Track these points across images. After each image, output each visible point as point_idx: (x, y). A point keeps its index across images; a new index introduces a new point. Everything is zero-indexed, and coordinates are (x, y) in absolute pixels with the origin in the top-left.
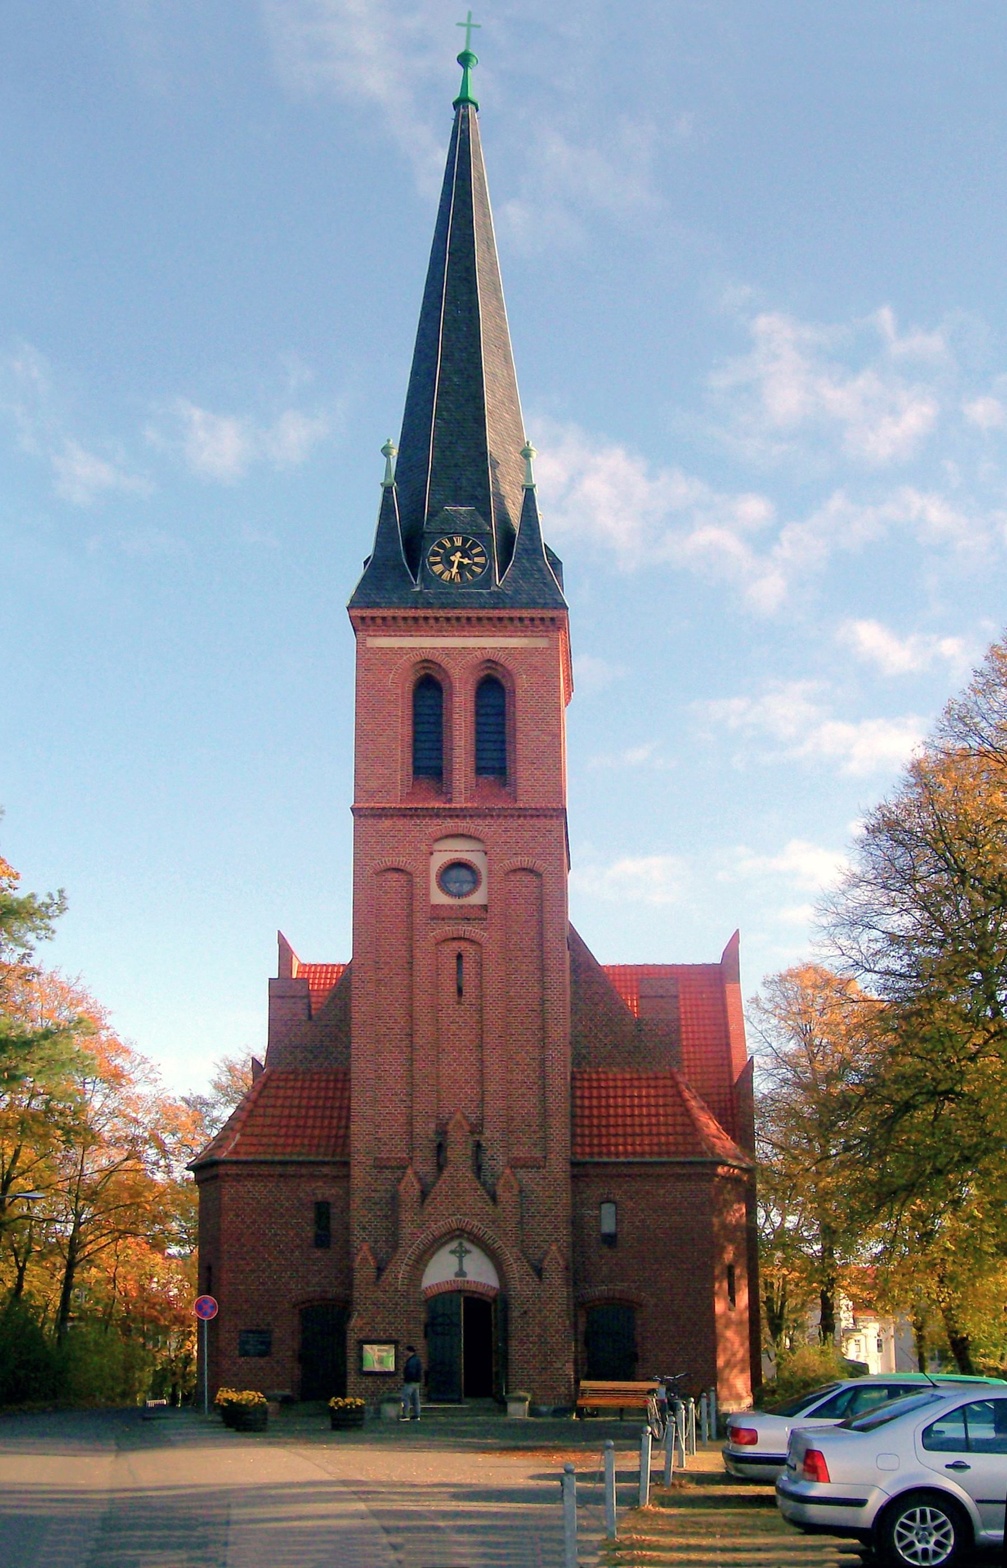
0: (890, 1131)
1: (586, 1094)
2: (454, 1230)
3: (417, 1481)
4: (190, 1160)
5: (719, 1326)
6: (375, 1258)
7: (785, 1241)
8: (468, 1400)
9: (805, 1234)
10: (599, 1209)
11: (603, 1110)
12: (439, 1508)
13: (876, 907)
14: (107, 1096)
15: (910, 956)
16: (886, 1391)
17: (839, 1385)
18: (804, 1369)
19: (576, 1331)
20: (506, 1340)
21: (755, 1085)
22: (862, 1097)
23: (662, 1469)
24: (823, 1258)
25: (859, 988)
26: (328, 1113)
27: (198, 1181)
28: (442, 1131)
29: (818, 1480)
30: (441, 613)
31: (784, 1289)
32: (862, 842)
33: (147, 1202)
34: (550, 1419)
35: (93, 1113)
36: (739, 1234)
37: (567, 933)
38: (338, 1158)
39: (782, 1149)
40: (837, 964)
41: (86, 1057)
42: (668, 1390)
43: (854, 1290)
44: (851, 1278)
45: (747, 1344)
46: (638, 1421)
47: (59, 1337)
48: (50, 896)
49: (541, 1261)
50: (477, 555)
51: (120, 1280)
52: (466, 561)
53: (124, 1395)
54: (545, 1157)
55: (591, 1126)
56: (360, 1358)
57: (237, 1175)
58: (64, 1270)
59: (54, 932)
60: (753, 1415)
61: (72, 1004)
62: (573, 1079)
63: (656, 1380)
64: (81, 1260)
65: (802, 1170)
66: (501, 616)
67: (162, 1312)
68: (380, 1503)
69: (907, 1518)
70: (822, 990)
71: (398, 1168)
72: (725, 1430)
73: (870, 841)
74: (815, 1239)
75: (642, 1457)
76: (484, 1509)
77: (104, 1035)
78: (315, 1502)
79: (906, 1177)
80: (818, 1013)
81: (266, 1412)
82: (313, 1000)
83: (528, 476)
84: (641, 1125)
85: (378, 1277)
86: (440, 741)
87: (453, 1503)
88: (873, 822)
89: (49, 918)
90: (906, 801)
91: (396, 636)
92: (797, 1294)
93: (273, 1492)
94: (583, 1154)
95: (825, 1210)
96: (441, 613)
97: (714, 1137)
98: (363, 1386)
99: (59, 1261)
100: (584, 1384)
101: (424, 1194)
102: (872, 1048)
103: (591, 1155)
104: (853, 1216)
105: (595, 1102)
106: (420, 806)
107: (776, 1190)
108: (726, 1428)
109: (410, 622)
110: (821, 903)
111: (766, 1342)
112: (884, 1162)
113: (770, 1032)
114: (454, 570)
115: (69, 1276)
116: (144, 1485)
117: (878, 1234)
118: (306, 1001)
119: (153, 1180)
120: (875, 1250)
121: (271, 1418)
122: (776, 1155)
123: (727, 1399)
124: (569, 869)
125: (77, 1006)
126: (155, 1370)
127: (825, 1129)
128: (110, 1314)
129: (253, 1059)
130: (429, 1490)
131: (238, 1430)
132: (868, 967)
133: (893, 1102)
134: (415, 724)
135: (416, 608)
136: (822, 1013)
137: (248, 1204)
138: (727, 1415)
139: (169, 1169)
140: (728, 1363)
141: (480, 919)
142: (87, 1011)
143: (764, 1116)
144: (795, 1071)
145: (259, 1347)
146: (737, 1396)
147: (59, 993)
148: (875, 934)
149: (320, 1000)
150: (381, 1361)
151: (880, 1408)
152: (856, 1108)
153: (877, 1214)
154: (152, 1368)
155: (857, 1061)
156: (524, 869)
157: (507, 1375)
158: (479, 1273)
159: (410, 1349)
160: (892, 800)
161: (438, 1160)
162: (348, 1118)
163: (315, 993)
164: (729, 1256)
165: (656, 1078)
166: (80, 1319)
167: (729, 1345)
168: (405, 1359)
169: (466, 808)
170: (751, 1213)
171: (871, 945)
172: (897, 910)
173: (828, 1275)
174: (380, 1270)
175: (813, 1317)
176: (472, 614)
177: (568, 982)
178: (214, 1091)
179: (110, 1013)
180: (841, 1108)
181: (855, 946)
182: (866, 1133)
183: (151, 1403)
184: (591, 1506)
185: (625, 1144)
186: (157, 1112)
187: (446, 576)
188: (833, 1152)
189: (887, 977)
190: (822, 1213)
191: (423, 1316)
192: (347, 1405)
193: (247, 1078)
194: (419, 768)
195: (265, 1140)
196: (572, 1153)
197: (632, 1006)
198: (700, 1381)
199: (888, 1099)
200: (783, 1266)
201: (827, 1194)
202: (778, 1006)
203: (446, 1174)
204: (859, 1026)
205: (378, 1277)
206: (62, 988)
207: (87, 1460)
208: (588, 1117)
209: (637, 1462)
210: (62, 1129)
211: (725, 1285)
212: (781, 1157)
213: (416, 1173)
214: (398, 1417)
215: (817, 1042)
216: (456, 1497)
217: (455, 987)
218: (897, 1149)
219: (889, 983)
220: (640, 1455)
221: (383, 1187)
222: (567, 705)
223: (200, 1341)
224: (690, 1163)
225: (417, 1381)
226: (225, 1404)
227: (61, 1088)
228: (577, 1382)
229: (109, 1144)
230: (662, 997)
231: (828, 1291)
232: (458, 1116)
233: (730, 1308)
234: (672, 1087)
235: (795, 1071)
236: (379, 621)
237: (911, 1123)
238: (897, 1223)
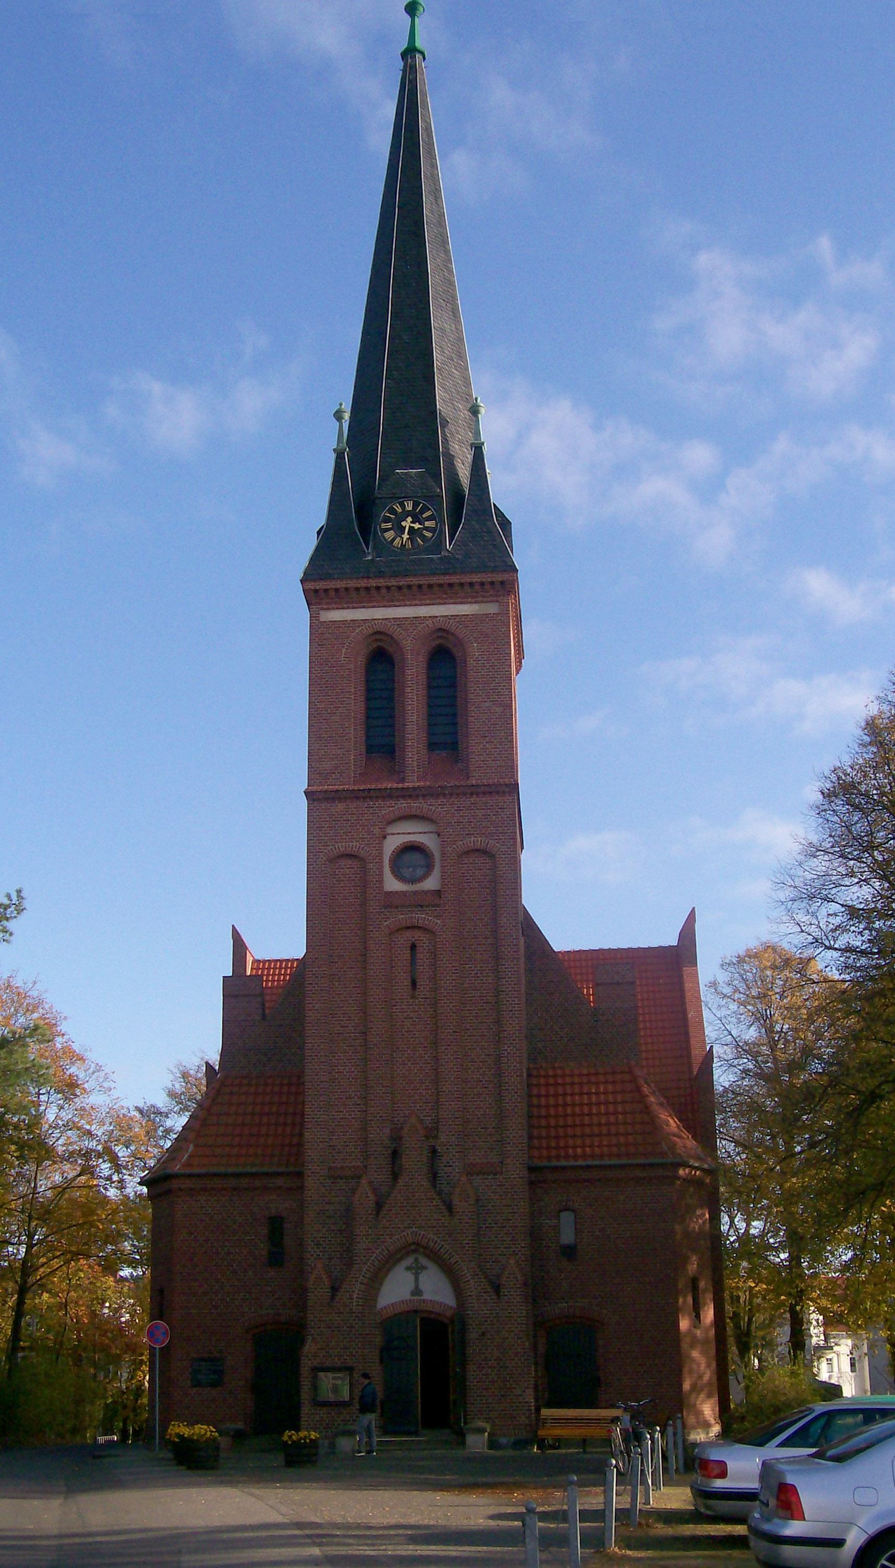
0: (856, 1124)
1: (543, 1092)
2: (410, 1245)
3: (374, 1522)
4: (143, 1174)
5: (684, 1346)
6: (330, 1277)
7: (751, 1248)
8: (425, 1432)
9: (771, 1241)
10: (558, 1218)
11: (560, 1109)
12: (396, 1553)
13: (834, 878)
14: (61, 1108)
15: (870, 931)
16: (861, 1416)
17: (812, 1410)
18: (774, 1392)
19: (536, 1354)
20: (463, 1364)
21: (715, 1077)
22: (826, 1088)
23: (628, 1506)
24: (790, 1267)
25: (819, 968)
26: (281, 1120)
27: (151, 1196)
28: (397, 1137)
29: (793, 1519)
30: (393, 582)
31: (750, 1303)
32: (818, 807)
33: (99, 1221)
34: (510, 1452)
35: (47, 1126)
36: (702, 1242)
37: (521, 918)
38: (292, 1169)
39: (745, 1147)
40: (796, 942)
41: (41, 1066)
42: (632, 1417)
43: (824, 1302)
44: (820, 1289)
45: (714, 1365)
46: (602, 1453)
47: (10, 1369)
48: (9, 896)
49: (499, 1276)
50: (428, 519)
51: (72, 1305)
52: (417, 526)
53: (74, 1431)
54: (502, 1162)
55: (548, 1127)
56: (315, 1387)
57: (191, 1189)
58: (16, 1296)
59: (11, 934)
60: (722, 1445)
61: (28, 1010)
62: (529, 1075)
63: (619, 1407)
64: (33, 1285)
65: (766, 1170)
66: (452, 581)
67: (113, 1340)
68: (334, 1548)
69: (888, 1560)
70: (782, 971)
71: (353, 1178)
72: (693, 1464)
73: (826, 807)
74: (782, 1247)
75: (607, 1493)
76: (442, 1553)
77: (59, 1042)
78: (267, 1547)
79: (874, 1176)
80: (777, 996)
81: (217, 1448)
82: (268, 998)
83: (477, 434)
84: (600, 1125)
85: (333, 1297)
86: (392, 717)
87: (411, 1547)
88: (828, 786)
89: (7, 919)
90: (861, 761)
91: (348, 608)
92: (764, 1308)
93: (225, 1536)
94: (540, 1158)
95: (791, 1213)
96: (393, 582)
97: (674, 1135)
98: (317, 1418)
99: (11, 1286)
100: (545, 1412)
101: (379, 1206)
102: (835, 1033)
103: (549, 1158)
104: (819, 1220)
105: (552, 1101)
106: (373, 787)
107: (740, 1193)
108: (694, 1460)
109: (363, 593)
110: (778, 875)
111: (734, 1362)
112: (851, 1159)
113: (729, 1018)
114: (406, 536)
115: (20, 1303)
116: (93, 1529)
117: (847, 1240)
118: (259, 999)
119: (106, 1197)
120: (844, 1258)
121: (223, 1454)
122: (739, 1154)
123: (694, 1428)
124: (522, 848)
125: (33, 1012)
126: (106, 1404)
127: (788, 1124)
128: (61, 1343)
129: (207, 1063)
130: (386, 1532)
131: (189, 1468)
132: (828, 944)
133: (858, 1092)
134: (368, 700)
135: (368, 578)
136: (782, 997)
137: (202, 1221)
138: (695, 1445)
139: (121, 1185)
140: (694, 1387)
141: (433, 906)
142: (43, 1018)
143: (726, 1112)
144: (757, 1061)
145: (212, 1376)
146: (705, 1424)
147: (16, 998)
148: (834, 907)
149: (274, 997)
150: (335, 1389)
151: (856, 1435)
152: (820, 1101)
153: (846, 1217)
154: (103, 1401)
155: (820, 1048)
156: (478, 850)
157: (465, 1403)
158: (436, 1291)
159: (365, 1376)
160: (847, 761)
161: (393, 1168)
162: (302, 1125)
163: (269, 991)
164: (693, 1267)
165: (614, 1073)
166: (31, 1348)
167: (695, 1367)
168: (360, 1387)
169: (418, 787)
170: (715, 1220)
171: (831, 919)
172: (856, 880)
173: (797, 1287)
174: (334, 1289)
175: (782, 1334)
176: (423, 581)
177: (522, 971)
178: (167, 1099)
179: (65, 1018)
180: (804, 1100)
181: (815, 921)
182: (831, 1127)
183: (101, 1439)
184: (554, 1549)
185: (583, 1146)
186: (111, 1124)
187: (397, 542)
188: (798, 1149)
189: (848, 954)
190: (788, 1218)
191: (378, 1340)
192: (301, 1439)
193: (201, 1084)
194: (371, 746)
195: (218, 1151)
196: (529, 1157)
197: (588, 994)
198: (668, 1409)
199: (853, 1089)
200: (748, 1278)
201: (793, 1195)
202: (736, 990)
203: (401, 1182)
204: (820, 1009)
205: (333, 1297)
206: (19, 994)
207: (36, 1502)
208: (545, 1117)
209: (601, 1499)
210: (16, 1143)
211: (690, 1300)
212: (744, 1156)
213: (370, 1183)
214: (354, 1452)
215: (778, 1028)
216: (413, 1540)
217: (409, 980)
218: (864, 1144)
219: (850, 961)
220: (605, 1491)
221: (338, 1199)
222: (517, 673)
223: (152, 1371)
224: (651, 1165)
225: (373, 1412)
226: (177, 1440)
227: (16, 1100)
228: (538, 1410)
229: (63, 1159)
230: (618, 984)
231: (797, 1304)
232: (413, 1120)
233: (696, 1324)
234: (630, 1082)
235: (757, 1061)
236: (332, 593)
237: (878, 1115)
238: (866, 1226)
